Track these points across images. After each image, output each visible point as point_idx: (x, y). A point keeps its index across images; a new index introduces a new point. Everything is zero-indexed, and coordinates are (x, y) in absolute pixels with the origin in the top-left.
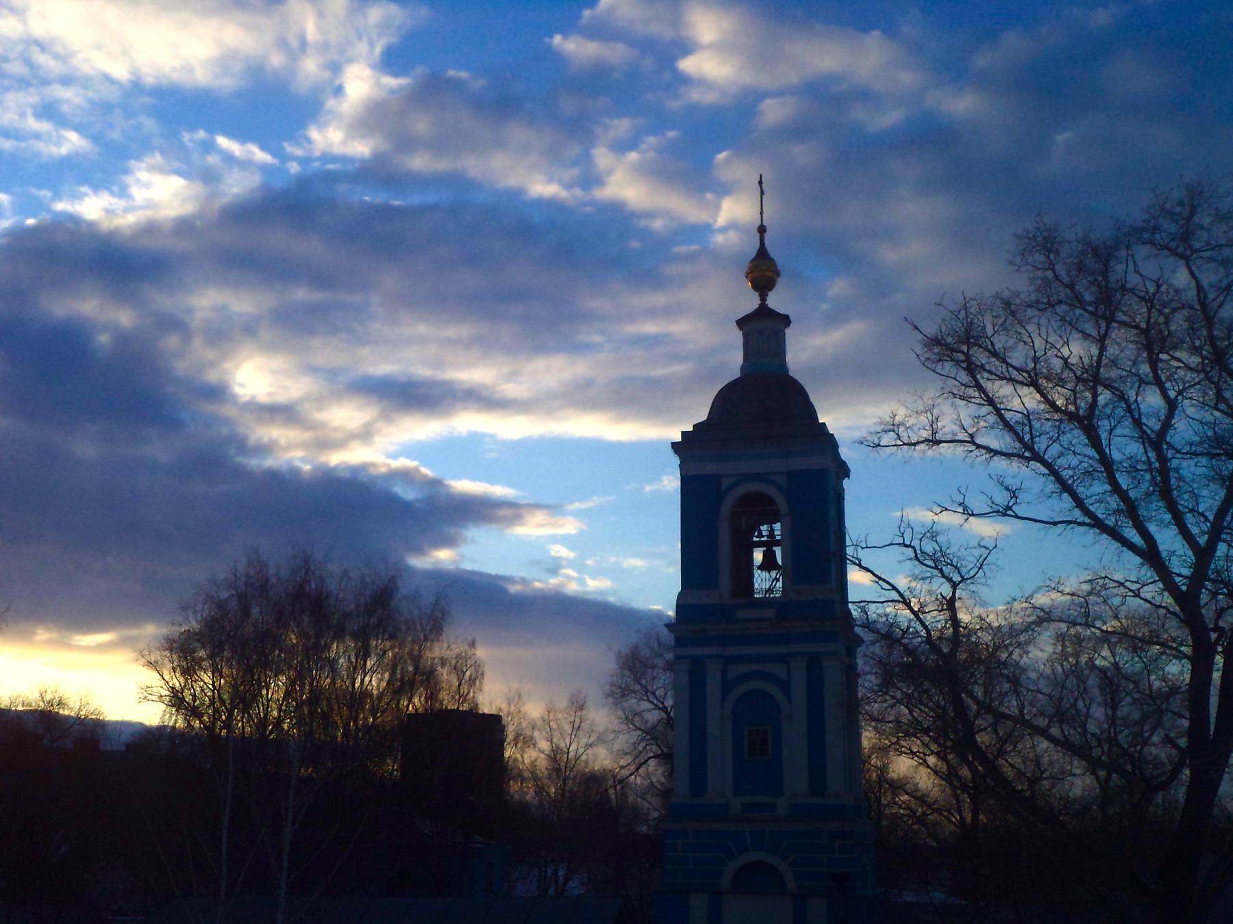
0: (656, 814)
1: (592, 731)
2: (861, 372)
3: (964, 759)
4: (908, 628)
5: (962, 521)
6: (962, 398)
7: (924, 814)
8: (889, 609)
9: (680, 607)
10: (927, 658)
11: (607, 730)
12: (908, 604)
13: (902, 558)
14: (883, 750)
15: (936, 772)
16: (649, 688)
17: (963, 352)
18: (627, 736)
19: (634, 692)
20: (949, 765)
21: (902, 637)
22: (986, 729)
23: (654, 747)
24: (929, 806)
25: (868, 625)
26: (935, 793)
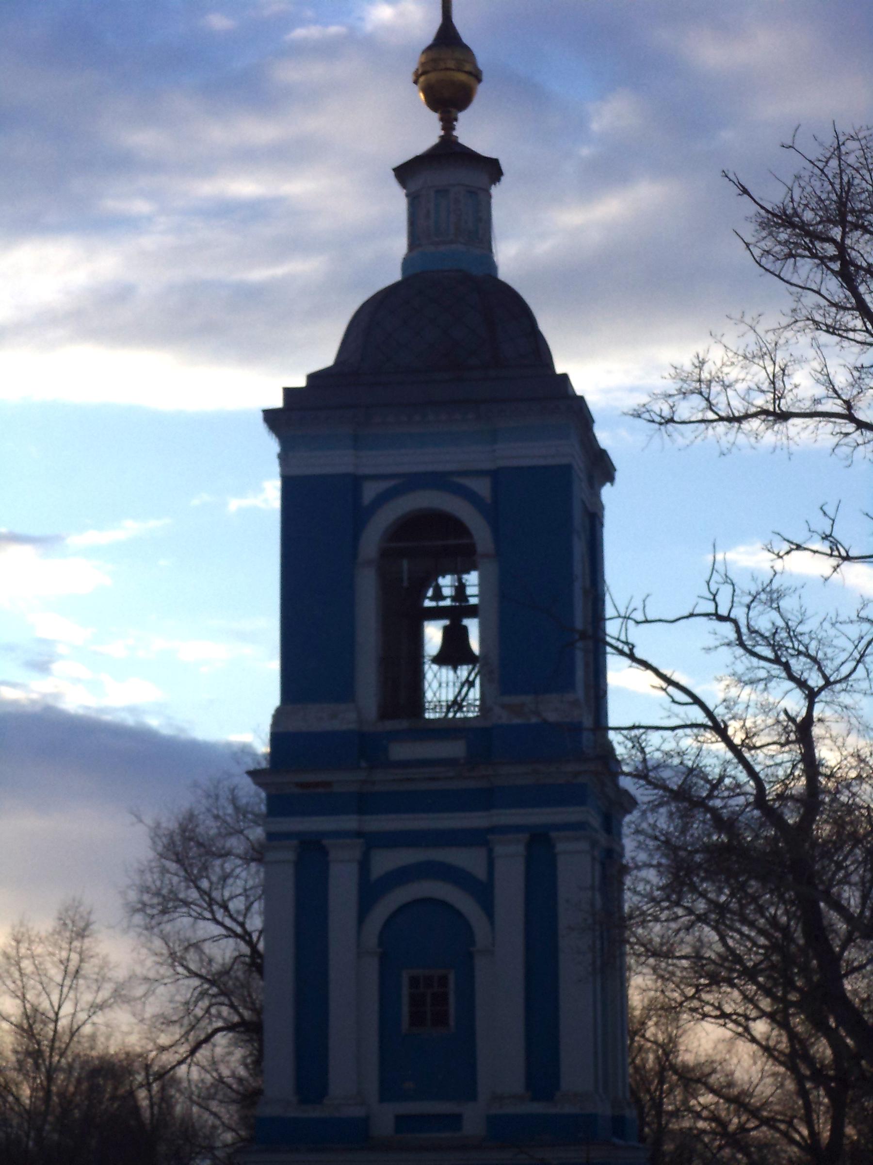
0: (229, 1137)
1: (101, 980)
2: (644, 280)
3: (819, 1025)
4: (721, 779)
5: (828, 571)
6: (831, 330)
7: (742, 1128)
8: (687, 742)
9: (276, 738)
10: (757, 837)
11: (132, 977)
12: (721, 730)
13: (712, 642)
14: (670, 1011)
15: (768, 1050)
16: (216, 894)
17: (832, 240)
18: (172, 988)
19: (186, 903)
20: (793, 1037)
21: (710, 796)
22: (862, 967)
23: (225, 1011)
24: (754, 1113)
25: (645, 773)
26: (766, 1089)
